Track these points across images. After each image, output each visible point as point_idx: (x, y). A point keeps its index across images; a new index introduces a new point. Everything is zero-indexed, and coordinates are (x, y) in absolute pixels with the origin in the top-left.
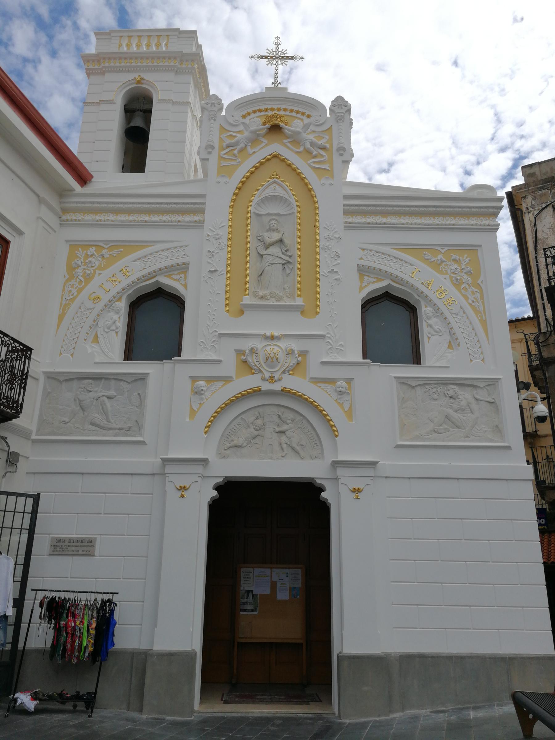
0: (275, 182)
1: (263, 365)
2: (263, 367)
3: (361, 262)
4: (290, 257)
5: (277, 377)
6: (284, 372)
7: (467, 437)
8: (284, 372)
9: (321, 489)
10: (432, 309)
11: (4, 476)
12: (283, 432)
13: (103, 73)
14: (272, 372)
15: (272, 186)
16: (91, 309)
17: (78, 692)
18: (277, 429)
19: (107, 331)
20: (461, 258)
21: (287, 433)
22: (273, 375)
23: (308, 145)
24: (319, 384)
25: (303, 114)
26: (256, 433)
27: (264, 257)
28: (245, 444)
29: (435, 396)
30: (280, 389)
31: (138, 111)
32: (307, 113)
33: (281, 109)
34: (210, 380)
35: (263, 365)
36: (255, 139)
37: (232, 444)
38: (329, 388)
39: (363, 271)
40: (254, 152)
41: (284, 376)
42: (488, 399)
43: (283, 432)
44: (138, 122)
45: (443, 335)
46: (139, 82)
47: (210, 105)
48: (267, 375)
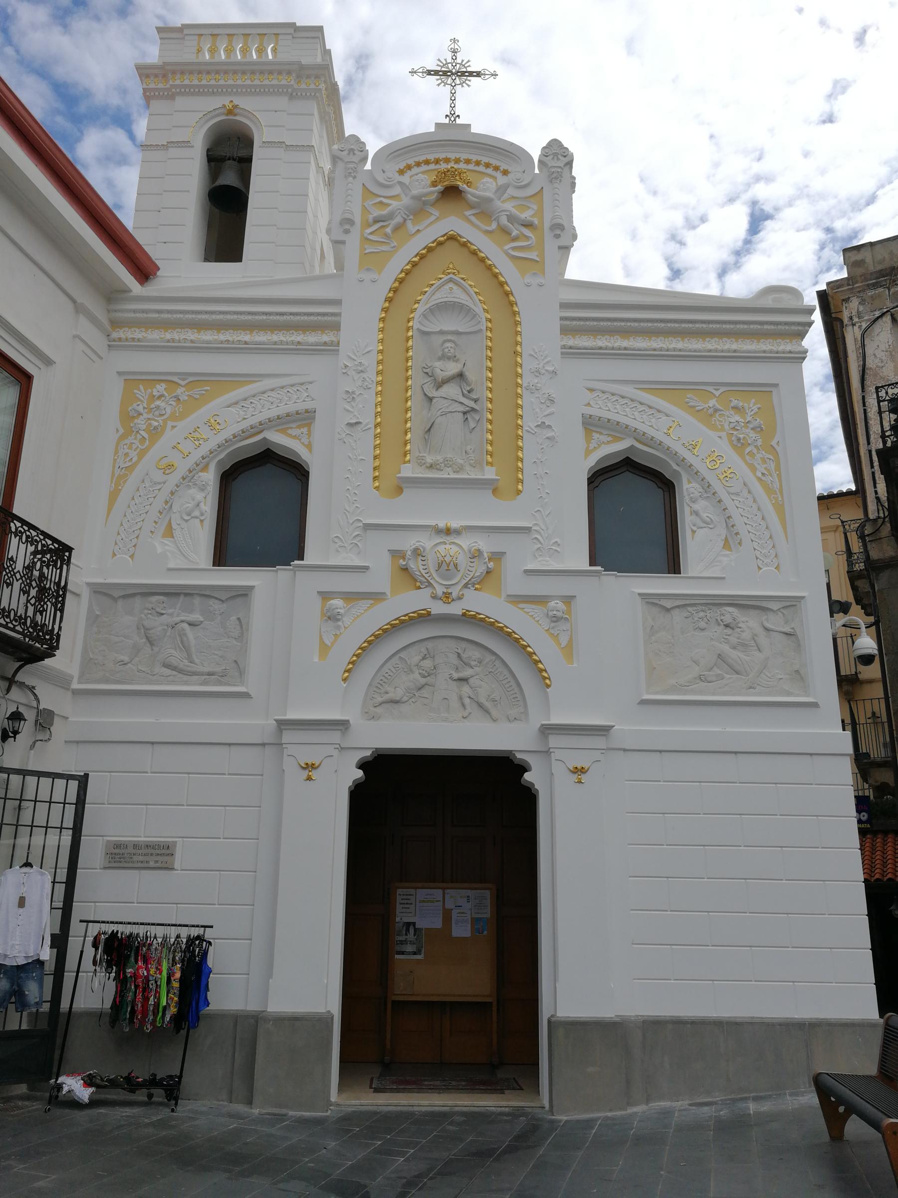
1: (434, 575)
3: (589, 411)
4: (476, 401)
6: (466, 586)
8: (466, 586)
9: (523, 768)
10: (698, 486)
11: (32, 747)
13: (172, 97)
15: (447, 287)
16: (160, 483)
18: (456, 676)
19: (187, 518)
21: (471, 681)
22: (449, 591)
23: (504, 220)
24: (521, 605)
26: (423, 681)
27: (434, 401)
29: (702, 624)
32: (503, 166)
35: (434, 575)
37: (386, 697)
38: (537, 610)
39: (591, 424)
44: (229, 178)
46: (230, 112)
48: (440, 591)
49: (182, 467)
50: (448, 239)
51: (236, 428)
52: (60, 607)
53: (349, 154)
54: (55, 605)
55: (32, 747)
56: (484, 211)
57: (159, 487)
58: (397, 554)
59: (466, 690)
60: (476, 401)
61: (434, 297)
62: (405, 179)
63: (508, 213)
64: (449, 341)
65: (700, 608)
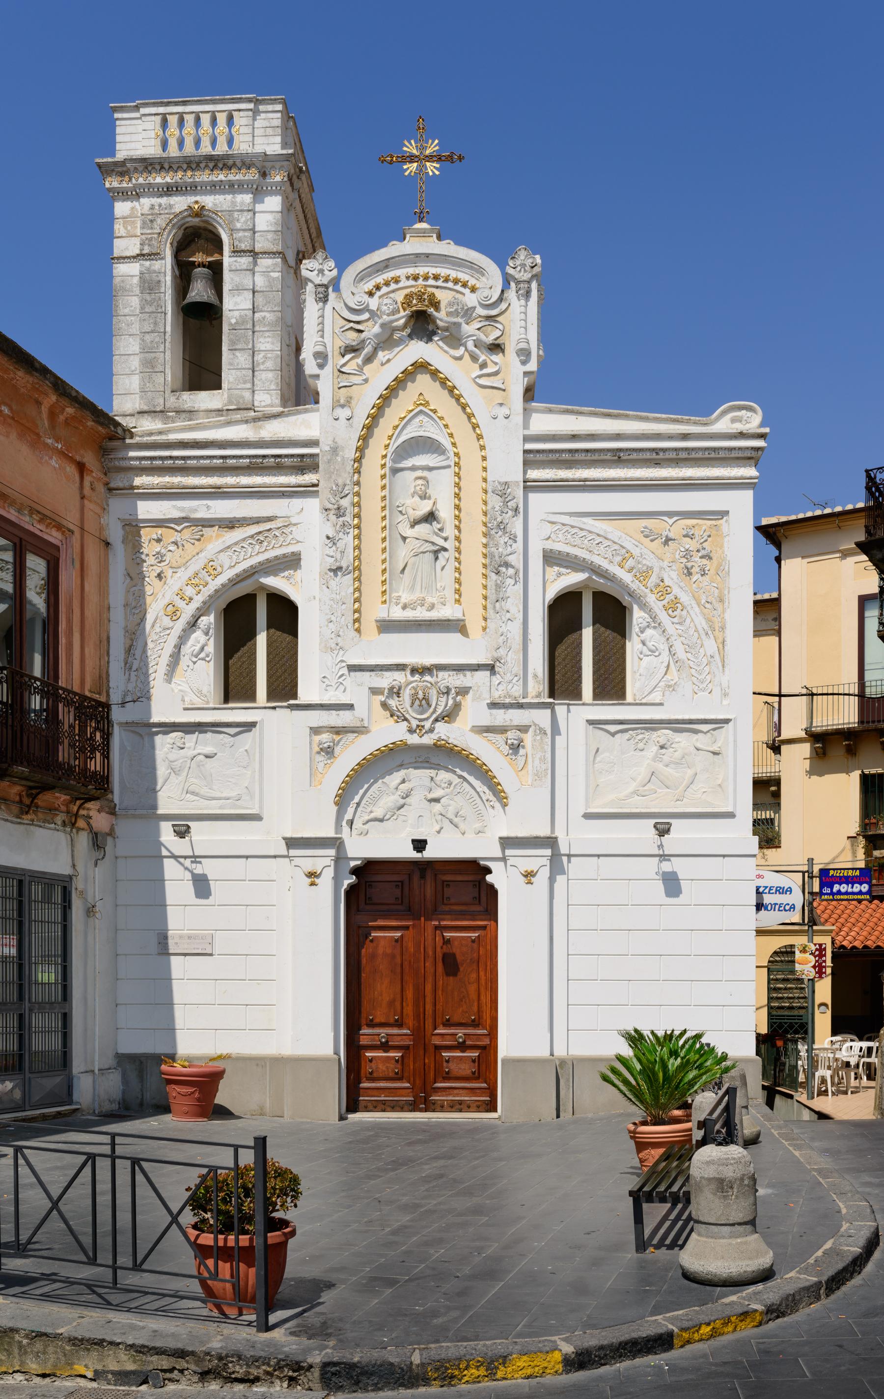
0: (421, 412)
1: (410, 712)
2: (408, 713)
3: (549, 545)
4: (446, 539)
5: (427, 725)
6: (436, 720)
7: (678, 800)
8: (436, 720)
9: (488, 871)
10: (646, 616)
11: (96, 865)
12: (437, 800)
13: (138, 196)
14: (420, 720)
15: (417, 420)
16: (168, 629)
17: (488, 871)
18: (430, 796)
19: (195, 659)
20: (223, 1207)
21: (442, 801)
22: (422, 723)
23: (470, 345)
24: (485, 734)
25: (465, 285)
26: (402, 801)
27: (407, 540)
28: (387, 817)
29: (641, 745)
30: (431, 742)
31: (199, 266)
32: (472, 282)
33: (430, 274)
34: (338, 731)
35: (409, 709)
36: (387, 341)
37: (372, 816)
38: (499, 738)
39: (551, 558)
40: (389, 361)
41: (438, 724)
42: (711, 749)
43: (437, 800)
44: (199, 291)
45: (660, 654)
46: (197, 215)
47: (316, 272)
48: (414, 723)
49: (188, 611)
50: (416, 368)
51: (228, 574)
52: (373, 1390)
53: (318, 275)
54: (102, 754)
55: (96, 865)
56: (454, 338)
57: (168, 632)
58: (375, 691)
59: (437, 807)
60: (446, 539)
61: (405, 432)
62: (373, 303)
63: (474, 338)
64: (420, 478)
65: (639, 731)
